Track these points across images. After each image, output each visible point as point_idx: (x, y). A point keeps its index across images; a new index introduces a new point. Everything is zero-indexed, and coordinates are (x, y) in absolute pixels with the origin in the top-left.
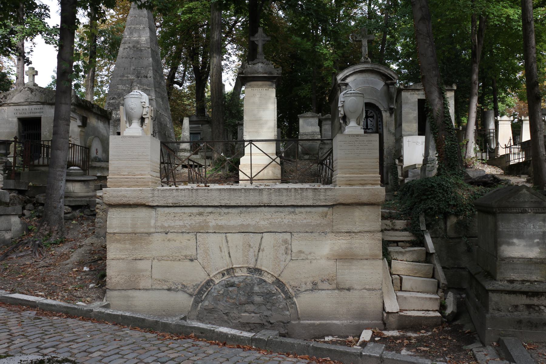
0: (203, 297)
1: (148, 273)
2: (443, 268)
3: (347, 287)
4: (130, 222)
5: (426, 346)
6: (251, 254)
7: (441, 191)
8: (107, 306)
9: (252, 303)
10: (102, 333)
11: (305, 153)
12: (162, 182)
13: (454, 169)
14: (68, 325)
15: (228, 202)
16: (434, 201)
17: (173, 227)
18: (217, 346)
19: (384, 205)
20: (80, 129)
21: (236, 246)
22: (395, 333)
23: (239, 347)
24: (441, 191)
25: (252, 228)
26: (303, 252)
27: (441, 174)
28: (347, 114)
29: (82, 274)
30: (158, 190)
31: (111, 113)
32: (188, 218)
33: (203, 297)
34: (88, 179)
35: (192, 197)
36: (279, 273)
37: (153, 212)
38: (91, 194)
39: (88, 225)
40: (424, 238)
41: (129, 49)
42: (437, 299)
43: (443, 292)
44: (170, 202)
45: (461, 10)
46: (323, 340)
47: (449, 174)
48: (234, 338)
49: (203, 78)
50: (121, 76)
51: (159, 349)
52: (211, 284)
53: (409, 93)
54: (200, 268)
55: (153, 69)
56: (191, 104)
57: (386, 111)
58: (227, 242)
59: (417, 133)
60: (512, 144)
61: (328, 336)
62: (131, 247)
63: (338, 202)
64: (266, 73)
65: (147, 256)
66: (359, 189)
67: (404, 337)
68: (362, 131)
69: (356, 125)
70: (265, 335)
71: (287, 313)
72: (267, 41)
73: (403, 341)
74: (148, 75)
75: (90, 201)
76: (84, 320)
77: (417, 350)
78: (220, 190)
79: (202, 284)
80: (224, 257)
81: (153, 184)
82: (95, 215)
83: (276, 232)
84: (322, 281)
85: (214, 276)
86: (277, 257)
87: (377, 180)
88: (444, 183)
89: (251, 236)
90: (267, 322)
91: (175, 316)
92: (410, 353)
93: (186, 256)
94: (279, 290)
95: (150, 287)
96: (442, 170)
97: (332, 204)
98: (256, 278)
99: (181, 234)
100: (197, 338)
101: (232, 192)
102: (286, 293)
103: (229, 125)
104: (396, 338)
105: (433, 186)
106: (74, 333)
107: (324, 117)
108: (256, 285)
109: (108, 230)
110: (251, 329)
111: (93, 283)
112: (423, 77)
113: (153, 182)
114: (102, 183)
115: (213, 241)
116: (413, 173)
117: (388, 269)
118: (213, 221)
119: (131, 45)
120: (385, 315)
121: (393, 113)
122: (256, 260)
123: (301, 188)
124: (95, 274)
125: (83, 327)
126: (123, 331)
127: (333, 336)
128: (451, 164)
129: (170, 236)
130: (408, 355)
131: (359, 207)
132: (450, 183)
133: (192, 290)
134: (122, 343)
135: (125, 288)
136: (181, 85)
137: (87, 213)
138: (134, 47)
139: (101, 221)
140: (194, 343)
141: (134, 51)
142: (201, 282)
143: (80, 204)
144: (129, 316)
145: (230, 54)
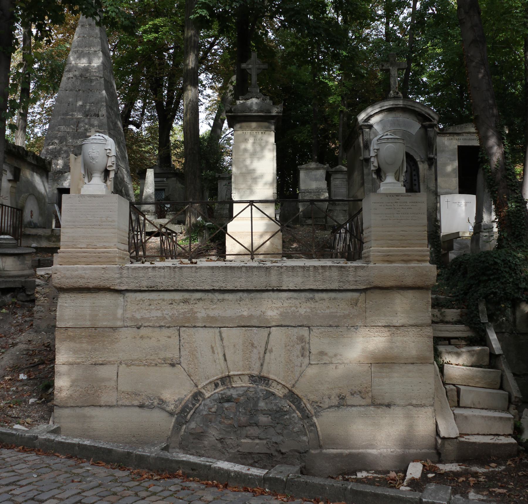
0: (189, 416)
1: (113, 384)
2: (514, 375)
3: (386, 402)
4: (89, 312)
5: (501, 487)
6: (255, 355)
7: (507, 269)
8: (56, 431)
9: (257, 425)
10: (53, 470)
11: (307, 215)
12: (131, 257)
13: (521, 240)
14: (4, 459)
15: (223, 285)
16: (498, 283)
17: (148, 320)
18: (216, 489)
19: (434, 290)
20: (10, 185)
21: (234, 346)
22: (454, 467)
23: (246, 490)
24: (507, 269)
25: (255, 320)
26: (326, 354)
27: (503, 247)
28: (381, 167)
29: (18, 384)
30: (128, 268)
31: (50, 163)
32: (169, 307)
33: (189, 416)
34: (24, 252)
35: (174, 278)
36: (293, 382)
37: (120, 299)
38: (26, 272)
39: (23, 315)
40: (486, 334)
41: (74, 78)
42: (509, 419)
43: (516, 409)
44: (145, 284)
45: (514, 29)
46: (354, 477)
47: (514, 246)
48: (239, 477)
49: (169, 116)
50: (63, 115)
51: (136, 494)
52: (199, 398)
53: (446, 138)
54: (184, 376)
55: (107, 106)
56: (151, 151)
57: (423, 162)
58: (222, 340)
59: (458, 192)
61: (360, 471)
62: (90, 347)
63: (374, 285)
64: (262, 112)
65: (111, 359)
66: (402, 267)
67: (468, 473)
68: (403, 190)
69: (396, 182)
70: (283, 472)
71: (305, 438)
72: (264, 69)
73: (467, 479)
74: (100, 113)
75: (25, 282)
76: (25, 451)
77: (491, 493)
78: (212, 268)
79: (186, 399)
80: (217, 361)
81: (121, 260)
82: (33, 301)
83: (288, 326)
84: (352, 394)
85: (204, 387)
86: (290, 360)
88: (510, 258)
89: (255, 331)
90: (277, 451)
91: (154, 445)
92: (482, 497)
93: (165, 360)
94: (294, 407)
95: (115, 403)
96: (505, 242)
97: (364, 287)
98: (261, 390)
99: (158, 329)
100: (186, 476)
101: (229, 271)
102: (302, 410)
103: (206, 179)
104: (457, 475)
105: (496, 263)
106: (13, 471)
107: (333, 169)
108: (261, 399)
109: (58, 324)
110: (255, 462)
111: (34, 397)
112: (477, 118)
113: (120, 257)
114: (47, 257)
115: (203, 338)
116: (460, 244)
117: (439, 376)
118: (203, 311)
119: (77, 73)
120: (440, 441)
121: (432, 164)
122: (262, 365)
123: (322, 266)
124: (36, 384)
125: (25, 462)
126: (81, 468)
127: (368, 471)
128: (517, 233)
129: (143, 331)
130: (479, 500)
131: (402, 292)
132: (518, 258)
133: (173, 407)
134: (84, 486)
135: (80, 405)
136: (138, 126)
137: (21, 298)
138: (81, 76)
139: (42, 309)
140: (184, 484)
141: (82, 81)
142: (186, 396)
143: (12, 286)
144: (90, 446)
145: (204, 86)
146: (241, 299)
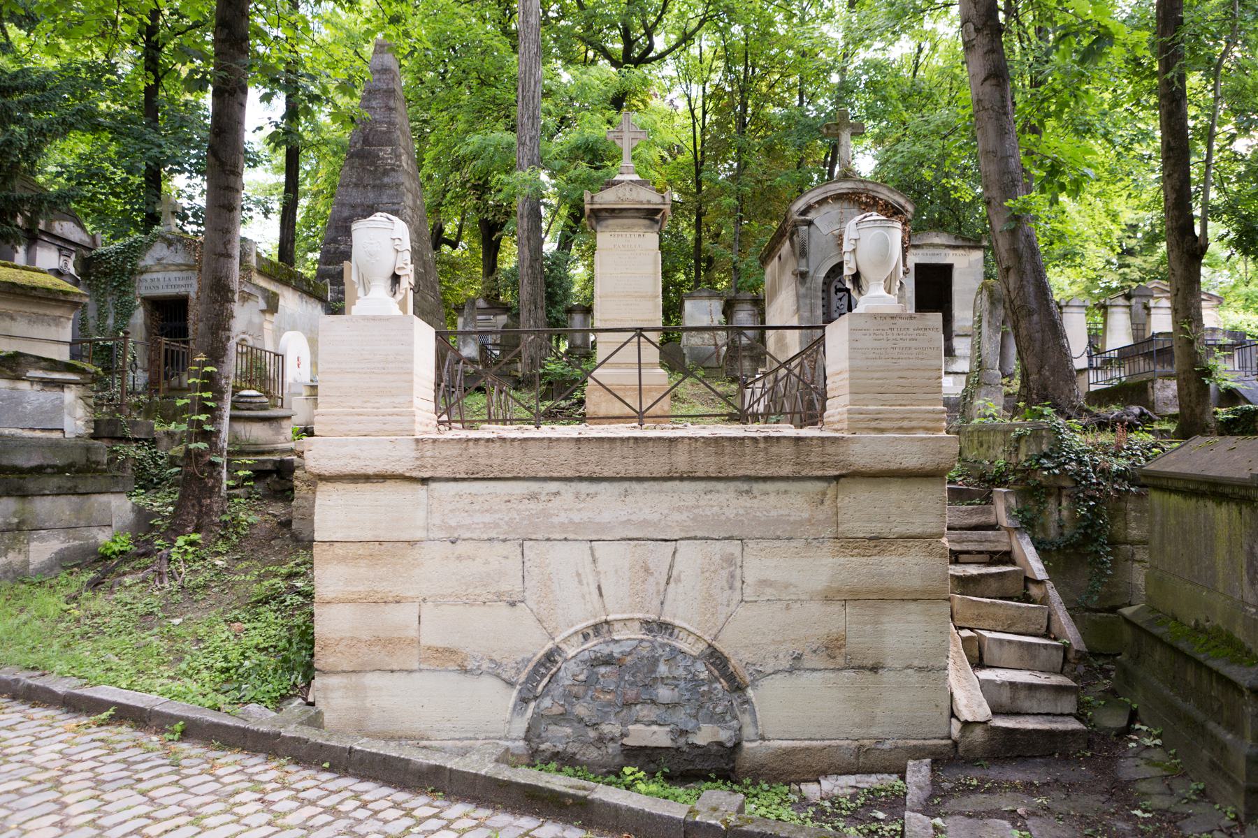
3: (870, 663)
146: (626, 493)
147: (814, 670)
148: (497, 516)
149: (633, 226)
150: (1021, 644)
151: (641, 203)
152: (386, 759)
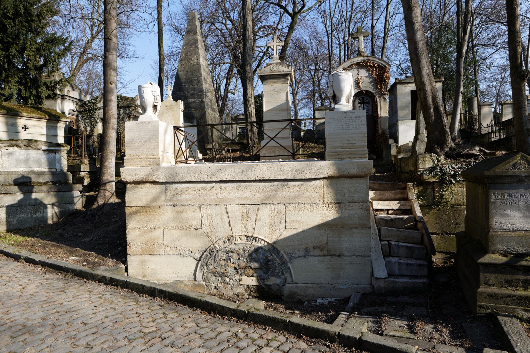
3: (338, 254)
59: (410, 117)
60: (493, 124)
87: (364, 154)
102: (282, 259)
146: (239, 187)
147: (314, 256)
148: (191, 196)
149: (278, 82)
150: (407, 247)
151: (280, 72)
152: (324, 331)
